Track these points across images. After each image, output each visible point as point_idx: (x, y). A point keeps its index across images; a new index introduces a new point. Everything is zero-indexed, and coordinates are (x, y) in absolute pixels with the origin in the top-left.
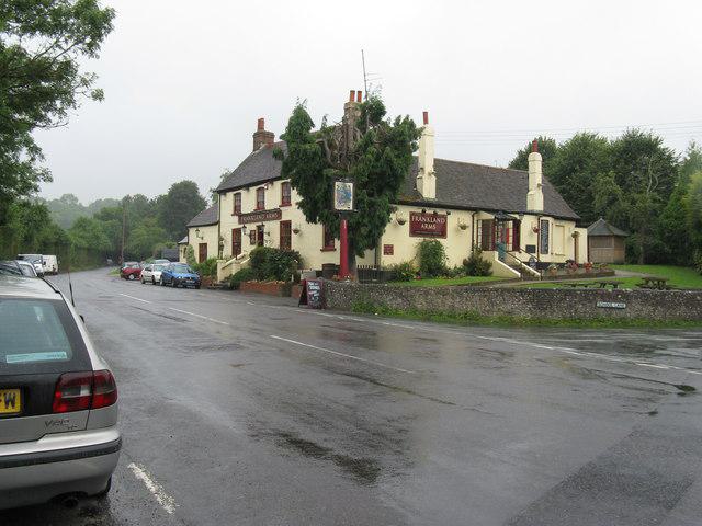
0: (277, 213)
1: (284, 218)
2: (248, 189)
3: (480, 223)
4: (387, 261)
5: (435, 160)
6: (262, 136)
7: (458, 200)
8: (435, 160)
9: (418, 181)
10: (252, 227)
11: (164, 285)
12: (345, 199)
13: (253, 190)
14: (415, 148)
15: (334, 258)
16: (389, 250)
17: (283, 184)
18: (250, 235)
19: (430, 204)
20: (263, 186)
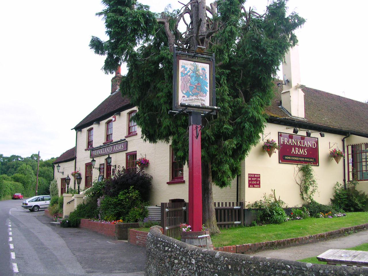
0: (124, 143)
1: (130, 149)
2: (99, 123)
3: (350, 148)
4: (252, 197)
5: (161, 203)
6: (97, 45)
7: (325, 121)
8: (161, 203)
9: (284, 98)
10: (100, 161)
11: (348, 133)
12: (198, 89)
13: (103, 122)
14: (279, 66)
15: (181, 192)
16: (255, 181)
17: (130, 113)
18: (100, 169)
19: (296, 124)
20: (111, 118)
